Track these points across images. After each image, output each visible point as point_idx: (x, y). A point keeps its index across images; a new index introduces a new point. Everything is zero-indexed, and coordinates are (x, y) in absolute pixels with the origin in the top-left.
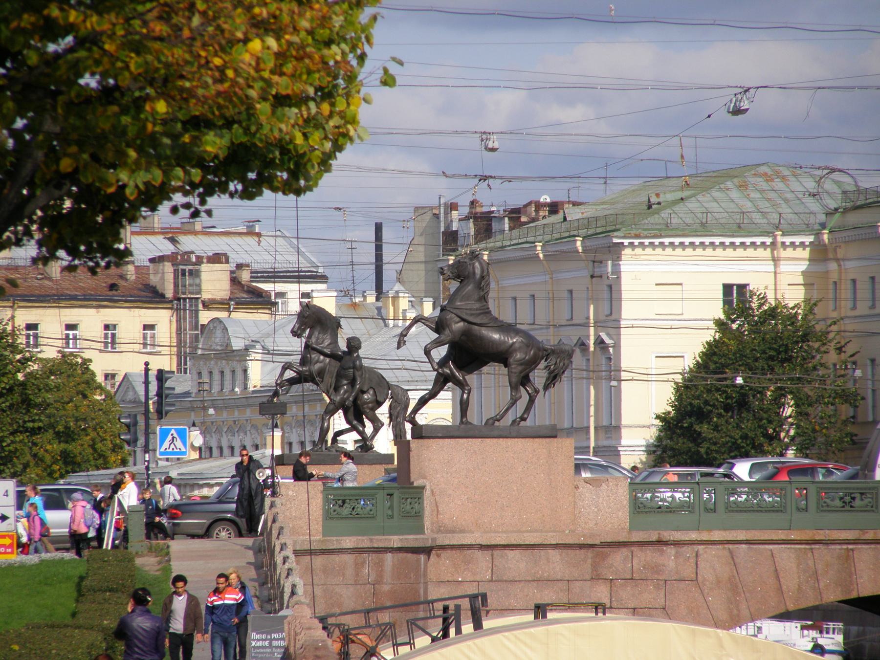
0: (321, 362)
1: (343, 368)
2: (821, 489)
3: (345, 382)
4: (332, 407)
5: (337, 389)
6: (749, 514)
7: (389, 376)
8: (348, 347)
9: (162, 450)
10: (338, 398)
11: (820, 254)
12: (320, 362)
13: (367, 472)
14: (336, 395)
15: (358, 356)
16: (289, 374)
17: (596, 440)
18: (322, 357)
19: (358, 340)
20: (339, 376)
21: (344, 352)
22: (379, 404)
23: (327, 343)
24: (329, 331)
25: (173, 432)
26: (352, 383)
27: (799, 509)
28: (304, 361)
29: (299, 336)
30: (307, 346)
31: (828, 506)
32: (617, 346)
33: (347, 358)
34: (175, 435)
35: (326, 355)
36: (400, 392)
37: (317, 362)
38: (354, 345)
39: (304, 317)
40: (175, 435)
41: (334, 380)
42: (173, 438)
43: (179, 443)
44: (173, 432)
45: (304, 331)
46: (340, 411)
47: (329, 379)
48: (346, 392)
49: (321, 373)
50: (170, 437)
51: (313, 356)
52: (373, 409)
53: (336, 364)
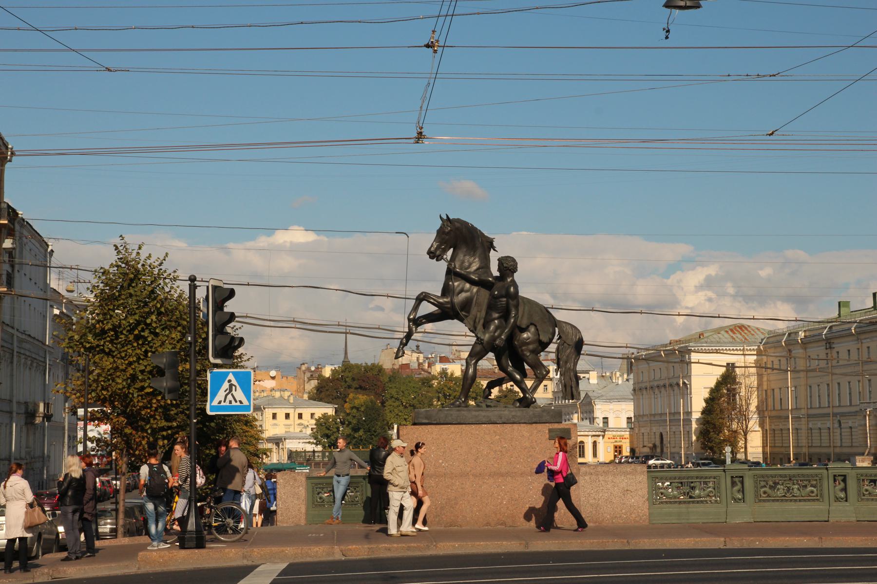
0: (467, 291)
1: (494, 298)
2: (316, 484)
3: (497, 315)
4: (479, 348)
5: (486, 326)
6: (777, 503)
7: (559, 316)
8: (499, 270)
9: (215, 403)
10: (487, 336)
11: (759, 353)
12: (465, 291)
13: (526, 434)
14: (484, 333)
15: (513, 281)
16: (427, 308)
17: (770, 425)
18: (468, 285)
19: (514, 260)
20: (491, 307)
21: (496, 278)
22: (544, 346)
23: (474, 267)
24: (478, 252)
25: (231, 377)
26: (505, 316)
27: (837, 499)
28: (446, 290)
29: (439, 258)
30: (451, 273)
31: (769, 496)
32: (690, 384)
33: (499, 284)
34: (234, 382)
35: (473, 283)
36: (570, 330)
37: (462, 291)
38: (508, 267)
39: (444, 233)
40: (234, 382)
41: (483, 313)
42: (231, 386)
43: (239, 394)
44: (231, 377)
45: (445, 251)
46: (491, 355)
47: (478, 312)
48: (497, 328)
49: (467, 305)
50: (226, 385)
51: (456, 284)
52: (536, 352)
53: (485, 294)
